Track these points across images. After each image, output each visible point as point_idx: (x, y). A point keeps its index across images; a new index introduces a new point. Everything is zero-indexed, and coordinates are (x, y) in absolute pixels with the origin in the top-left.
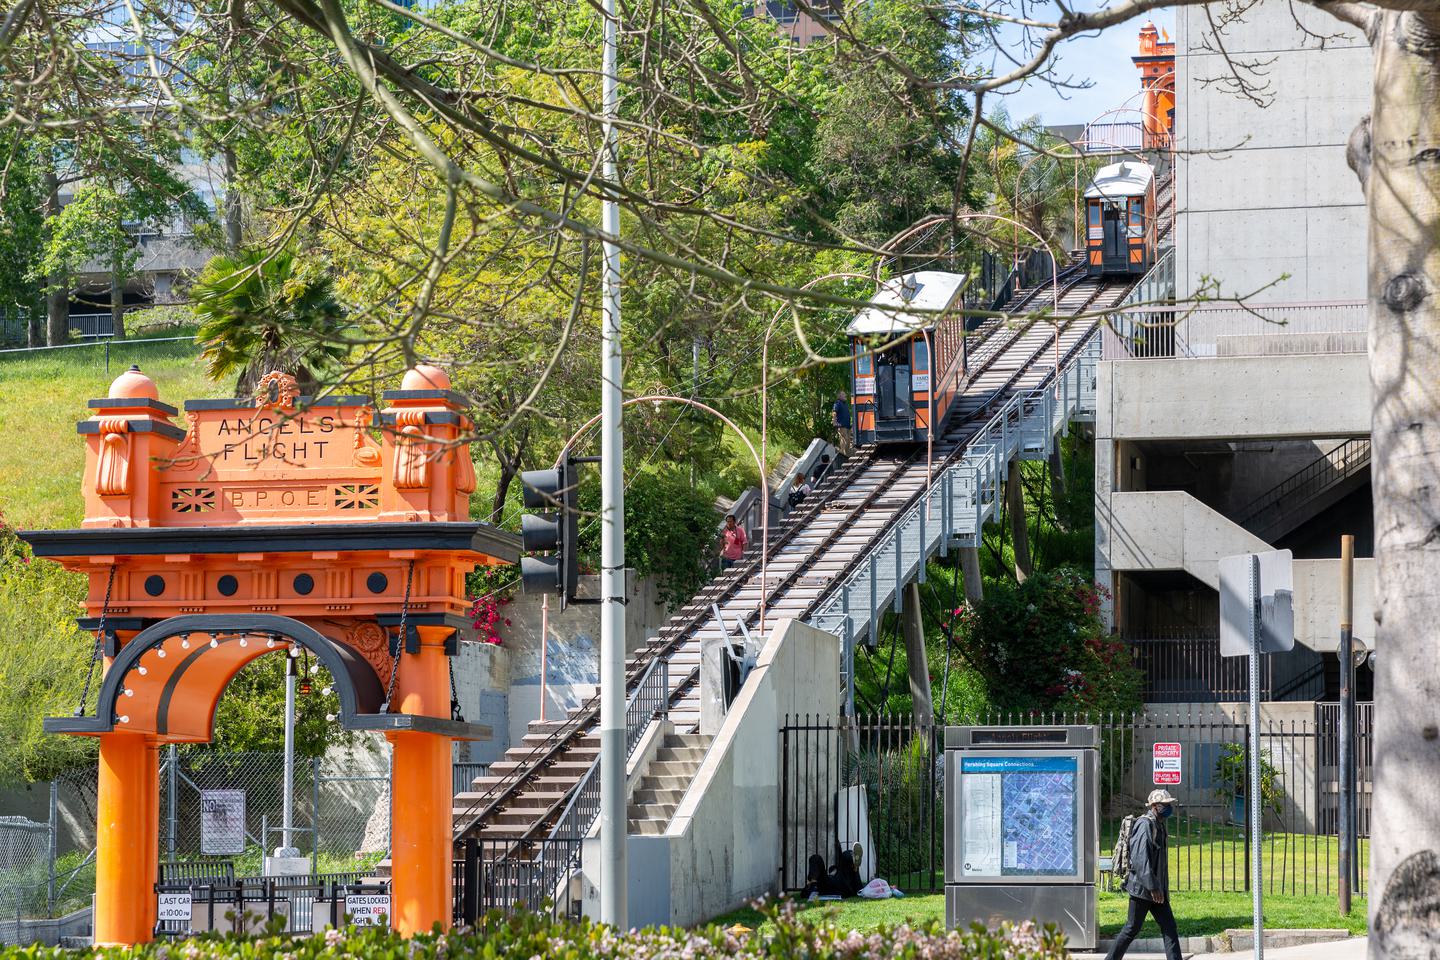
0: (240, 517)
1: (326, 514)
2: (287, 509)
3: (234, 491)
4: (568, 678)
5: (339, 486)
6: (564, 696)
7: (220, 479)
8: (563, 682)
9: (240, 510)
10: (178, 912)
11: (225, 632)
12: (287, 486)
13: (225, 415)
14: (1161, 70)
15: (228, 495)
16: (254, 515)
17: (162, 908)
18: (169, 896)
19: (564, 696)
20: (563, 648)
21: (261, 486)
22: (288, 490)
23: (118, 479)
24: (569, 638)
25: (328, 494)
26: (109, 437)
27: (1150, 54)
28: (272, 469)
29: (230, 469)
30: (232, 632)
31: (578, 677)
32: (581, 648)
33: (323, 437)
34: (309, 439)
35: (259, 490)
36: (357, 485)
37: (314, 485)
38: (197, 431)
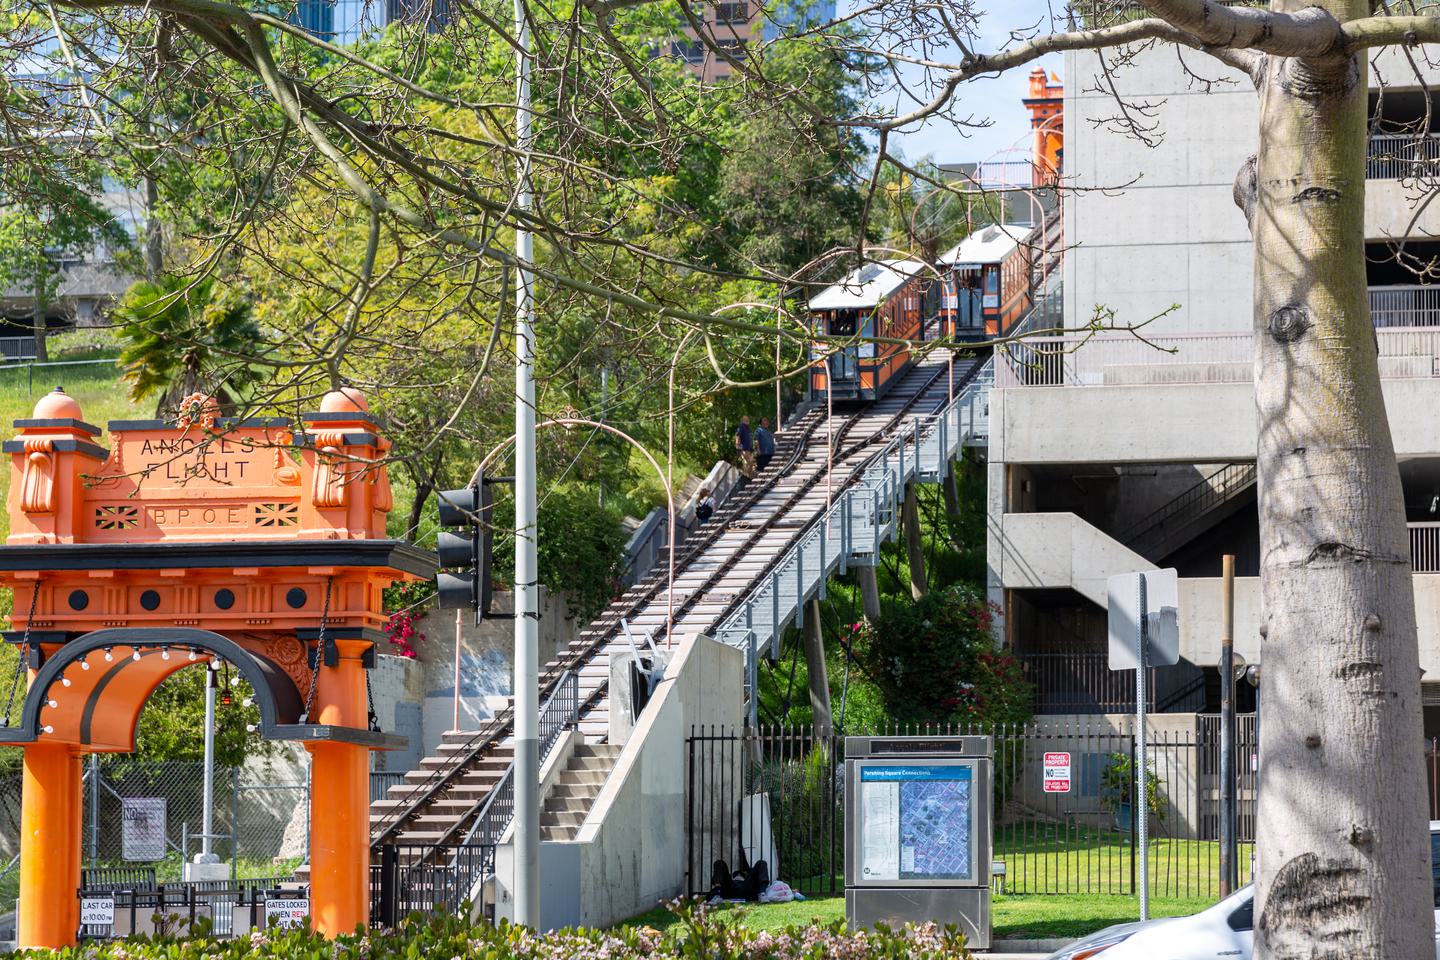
0: (163, 535)
2: (208, 526)
3: (157, 509)
4: (481, 690)
5: (259, 505)
6: (477, 707)
8: (476, 694)
9: (162, 527)
10: (101, 917)
11: (147, 645)
12: (208, 504)
13: (147, 436)
14: (1049, 112)
15: (151, 513)
16: (176, 532)
17: (85, 912)
18: (92, 901)
19: (477, 707)
20: (476, 661)
21: (183, 504)
22: (210, 508)
23: (43, 497)
24: (481, 652)
25: (249, 512)
26: (34, 456)
27: (1039, 97)
28: (198, 487)
29: (154, 488)
30: (154, 645)
31: (490, 689)
32: (493, 662)
33: (244, 457)
34: (230, 459)
35: (181, 508)
36: (277, 504)
37: (234, 503)
38: (120, 450)
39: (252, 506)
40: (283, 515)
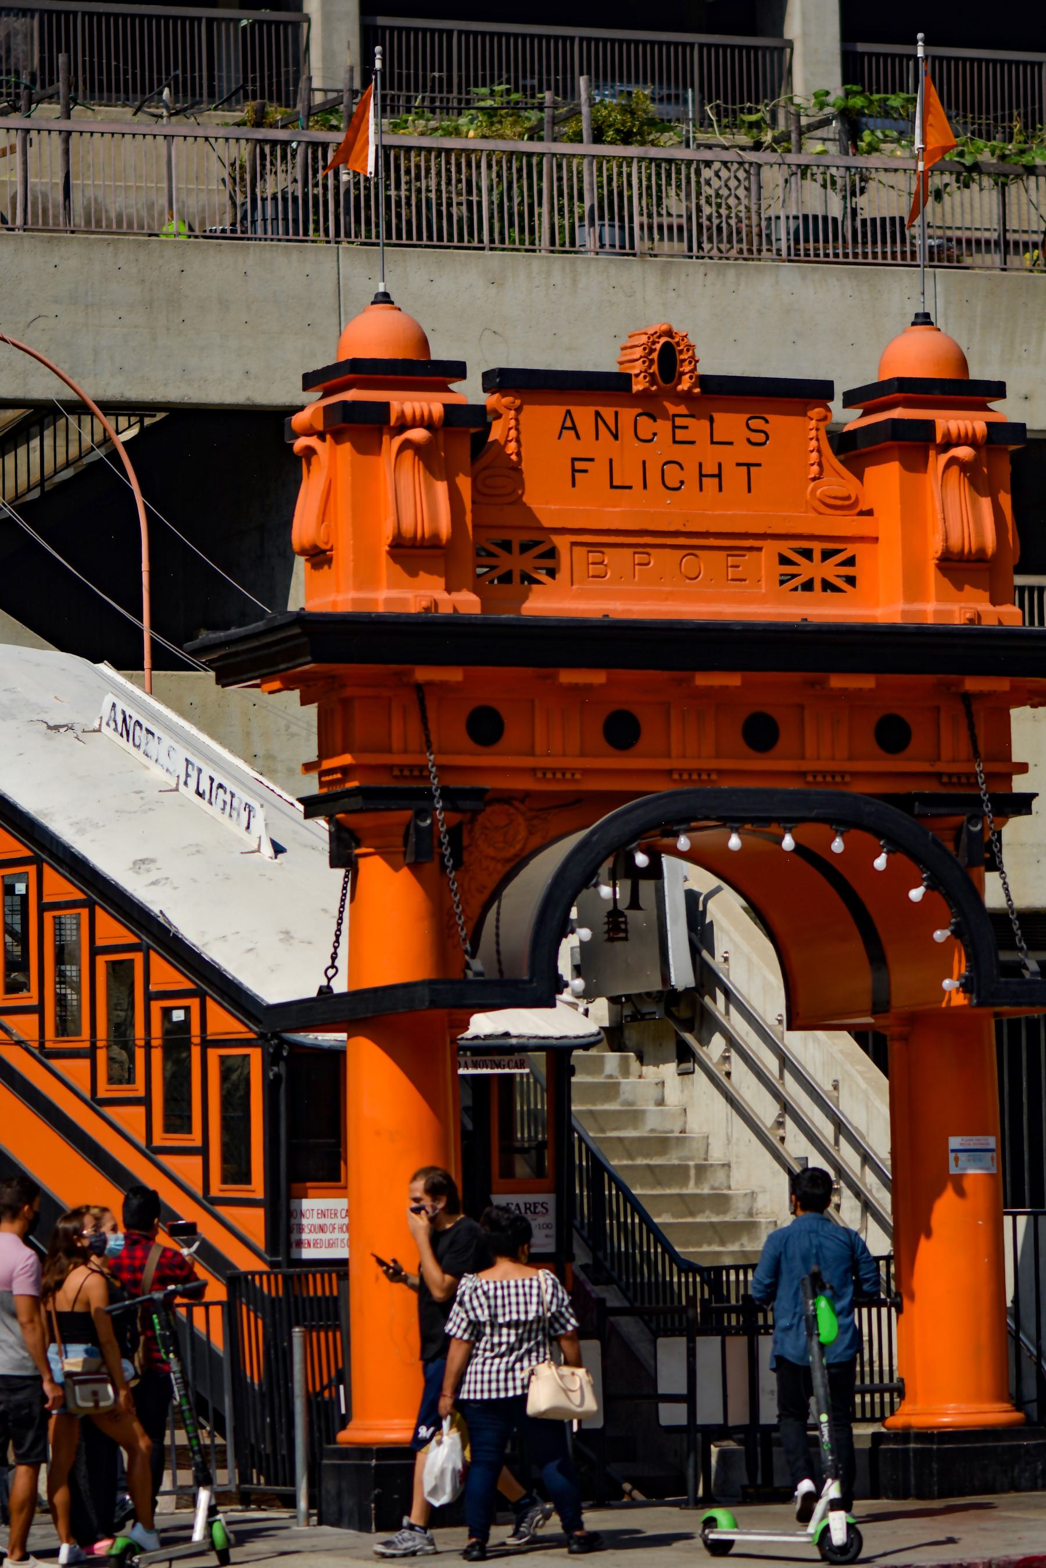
1: (762, 600)
5: (785, 547)
7: (546, 524)
33: (752, 455)
34: (729, 456)
37: (738, 542)
39: (771, 549)
40: (830, 570)
